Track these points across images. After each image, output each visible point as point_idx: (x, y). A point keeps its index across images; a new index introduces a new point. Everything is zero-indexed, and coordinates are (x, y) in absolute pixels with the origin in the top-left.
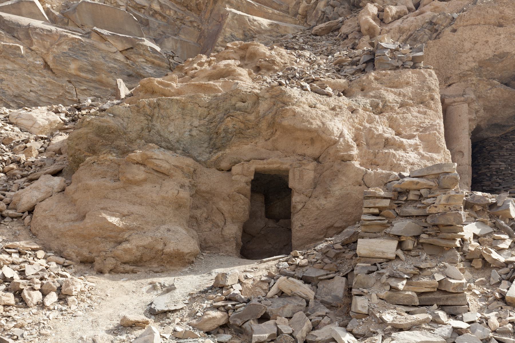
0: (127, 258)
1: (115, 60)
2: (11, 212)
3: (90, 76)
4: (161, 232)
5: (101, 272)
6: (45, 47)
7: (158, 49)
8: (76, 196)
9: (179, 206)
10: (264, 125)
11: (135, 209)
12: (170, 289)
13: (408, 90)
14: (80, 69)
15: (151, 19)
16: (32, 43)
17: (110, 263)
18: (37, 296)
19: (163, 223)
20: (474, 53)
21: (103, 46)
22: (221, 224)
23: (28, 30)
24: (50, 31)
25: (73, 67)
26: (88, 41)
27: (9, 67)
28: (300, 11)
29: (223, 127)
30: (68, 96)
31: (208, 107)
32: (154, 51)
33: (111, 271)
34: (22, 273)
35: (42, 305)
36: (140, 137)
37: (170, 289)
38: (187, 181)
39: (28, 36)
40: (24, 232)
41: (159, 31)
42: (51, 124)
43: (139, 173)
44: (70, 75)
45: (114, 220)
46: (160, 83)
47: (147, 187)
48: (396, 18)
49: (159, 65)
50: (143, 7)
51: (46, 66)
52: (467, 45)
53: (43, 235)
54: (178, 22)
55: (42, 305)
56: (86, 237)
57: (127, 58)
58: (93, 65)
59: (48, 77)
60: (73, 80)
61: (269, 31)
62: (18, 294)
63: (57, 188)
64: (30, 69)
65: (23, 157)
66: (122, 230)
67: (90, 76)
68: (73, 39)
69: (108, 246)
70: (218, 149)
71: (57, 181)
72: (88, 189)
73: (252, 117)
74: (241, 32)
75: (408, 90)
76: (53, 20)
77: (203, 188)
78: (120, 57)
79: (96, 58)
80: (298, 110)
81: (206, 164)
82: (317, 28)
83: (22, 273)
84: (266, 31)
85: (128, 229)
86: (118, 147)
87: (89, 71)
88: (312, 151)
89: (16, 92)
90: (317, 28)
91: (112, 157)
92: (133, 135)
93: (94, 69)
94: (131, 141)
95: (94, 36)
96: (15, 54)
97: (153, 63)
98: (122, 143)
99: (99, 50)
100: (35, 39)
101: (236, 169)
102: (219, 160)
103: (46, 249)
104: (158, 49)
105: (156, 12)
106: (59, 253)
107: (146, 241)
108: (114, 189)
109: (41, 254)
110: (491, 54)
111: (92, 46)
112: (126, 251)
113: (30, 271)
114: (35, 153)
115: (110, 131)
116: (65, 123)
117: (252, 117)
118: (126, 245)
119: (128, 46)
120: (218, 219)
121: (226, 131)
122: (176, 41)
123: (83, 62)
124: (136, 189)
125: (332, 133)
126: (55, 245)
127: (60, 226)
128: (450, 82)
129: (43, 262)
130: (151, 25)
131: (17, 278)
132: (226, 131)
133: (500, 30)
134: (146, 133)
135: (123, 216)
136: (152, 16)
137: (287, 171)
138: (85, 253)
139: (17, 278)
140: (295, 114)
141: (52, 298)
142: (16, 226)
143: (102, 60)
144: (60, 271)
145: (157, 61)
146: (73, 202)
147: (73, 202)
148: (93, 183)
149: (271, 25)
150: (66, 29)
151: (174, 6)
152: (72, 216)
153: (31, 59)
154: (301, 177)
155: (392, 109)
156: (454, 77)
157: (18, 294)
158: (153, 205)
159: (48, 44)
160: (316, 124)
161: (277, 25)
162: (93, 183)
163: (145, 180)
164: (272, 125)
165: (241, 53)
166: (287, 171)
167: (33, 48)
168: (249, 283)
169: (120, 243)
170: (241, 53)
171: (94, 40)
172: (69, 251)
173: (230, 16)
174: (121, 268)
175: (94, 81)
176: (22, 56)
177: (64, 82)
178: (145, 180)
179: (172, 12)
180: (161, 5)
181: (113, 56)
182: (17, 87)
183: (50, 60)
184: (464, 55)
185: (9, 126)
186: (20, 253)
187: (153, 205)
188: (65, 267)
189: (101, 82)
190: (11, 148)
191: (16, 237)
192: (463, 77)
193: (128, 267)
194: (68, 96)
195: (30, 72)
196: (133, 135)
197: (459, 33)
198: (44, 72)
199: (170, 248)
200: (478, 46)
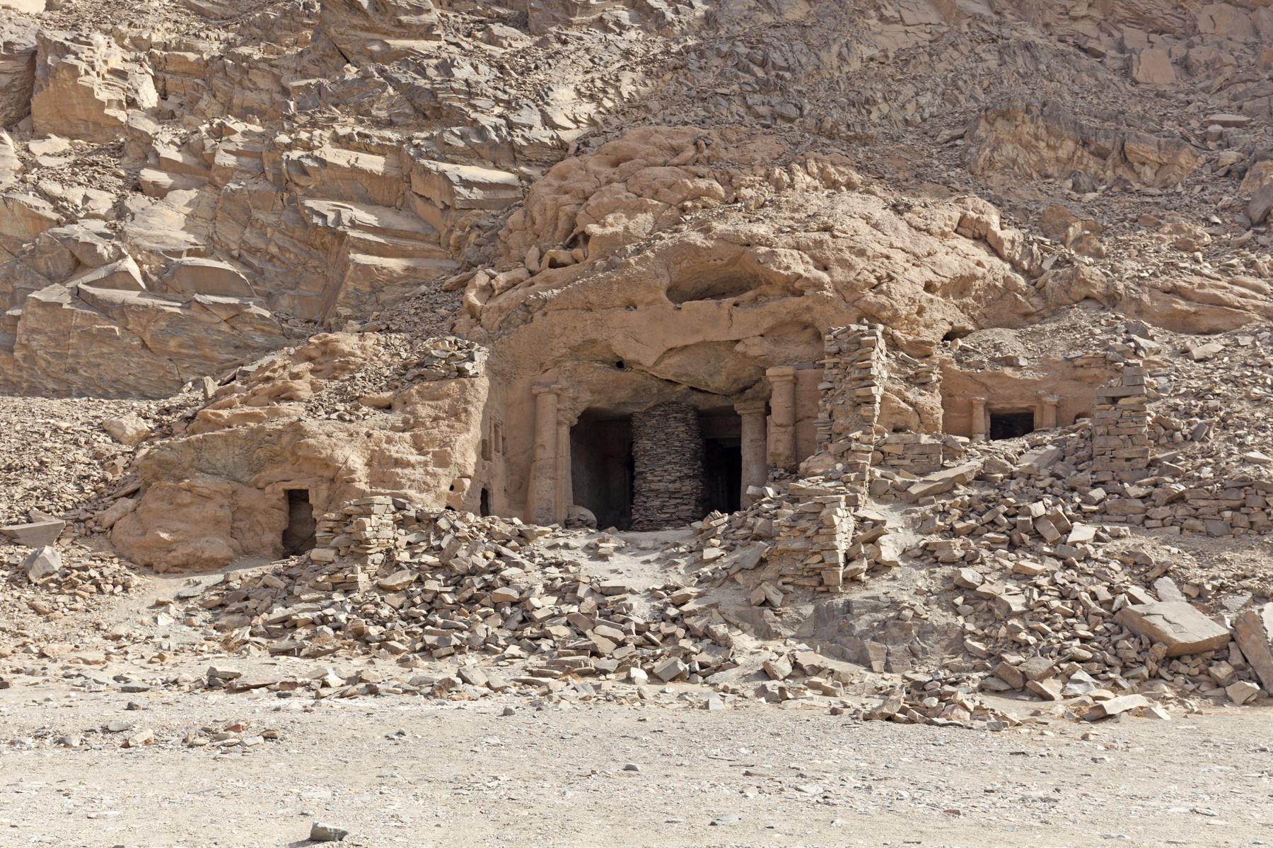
0: (176, 562)
1: (219, 331)
2: (98, 528)
3: (193, 352)
4: (201, 543)
5: (157, 573)
6: (141, 325)
7: (267, 314)
8: (143, 516)
9: (218, 522)
10: (287, 454)
11: (182, 526)
12: (197, 584)
13: (446, 403)
14: (181, 346)
15: (269, 267)
16: (128, 323)
17: (163, 566)
18: (109, 587)
19: (204, 536)
20: (564, 339)
21: (204, 317)
22: (260, 532)
23: (124, 307)
24: (146, 307)
25: (172, 344)
26: (187, 313)
27: (105, 350)
28: (452, 242)
29: (255, 456)
30: (169, 376)
31: (245, 438)
32: (262, 317)
33: (164, 572)
34: (101, 574)
35: (112, 593)
36: (192, 467)
37: (197, 584)
38: (226, 502)
39: (123, 315)
40: (107, 544)
41: (277, 281)
42: (138, 433)
43: (186, 498)
44: (170, 353)
45: (164, 536)
46: (213, 414)
47: (193, 508)
48: (506, 289)
49: (271, 333)
50: (259, 250)
51: (144, 345)
52: (558, 331)
53: (119, 546)
54: (300, 268)
55: (112, 593)
56: (147, 548)
57: (233, 328)
58: (194, 339)
59: (146, 357)
60: (174, 357)
61: (405, 277)
62: (98, 586)
63: (130, 508)
64: (127, 351)
65: (110, 476)
66: (171, 543)
67: (193, 352)
68: (171, 313)
69: (162, 554)
70: (256, 472)
71: (130, 503)
72: (150, 511)
73: (277, 448)
74: (367, 283)
75: (446, 403)
76: (151, 289)
77: (244, 505)
78: (225, 328)
79: (198, 332)
80: (311, 441)
81: (248, 485)
82: (447, 282)
83: (101, 574)
84: (400, 278)
85: (175, 541)
86: (174, 475)
87: (190, 347)
88: (328, 474)
89: (115, 376)
90: (447, 282)
91: (171, 483)
92: (186, 465)
93: (197, 343)
94: (185, 470)
95: (195, 307)
96: (110, 337)
97: (263, 331)
98: (177, 472)
99: (199, 322)
100: (130, 317)
101: (268, 489)
102: (256, 482)
103: (120, 556)
104: (267, 314)
105: (273, 257)
106: (129, 560)
107: (189, 550)
108: (168, 511)
109: (116, 560)
110: (580, 341)
111: (193, 319)
112: (174, 557)
113: (106, 572)
114: (120, 470)
115: (167, 462)
116: (152, 431)
117: (277, 448)
118: (173, 554)
119: (233, 313)
120: (258, 529)
121: (258, 458)
122: (293, 297)
123: (184, 338)
124: (185, 510)
125: (337, 461)
126: (127, 553)
127: (131, 540)
128: (545, 368)
129: (117, 566)
130: (267, 274)
131: (98, 577)
132: (258, 458)
133: (587, 315)
134: (196, 463)
135: (172, 532)
136: (270, 260)
137: (307, 491)
138: (147, 559)
139: (98, 577)
140: (308, 446)
141: (120, 588)
142: (101, 539)
143: (204, 334)
144: (127, 572)
145: (267, 329)
146: (140, 521)
147: (140, 521)
148: (153, 506)
149: (407, 269)
150: (164, 299)
151: (295, 246)
152: (139, 532)
153: (127, 340)
154: (317, 495)
155: (423, 424)
156: (548, 363)
157: (98, 586)
158: (196, 523)
159: (144, 321)
160: (326, 453)
161: (415, 269)
162: (153, 506)
163: (191, 503)
164: (294, 454)
165: (323, 348)
166: (307, 491)
167: (130, 327)
168: (247, 579)
169: (170, 551)
170: (323, 348)
171: (194, 311)
172: (136, 558)
173: (352, 267)
174: (172, 569)
175: (197, 357)
176: (118, 338)
177: (164, 361)
178: (191, 503)
179: (292, 256)
180: (280, 248)
181: (216, 327)
182: (115, 371)
183: (147, 338)
184: (555, 341)
185: (102, 435)
186: (102, 560)
187: (196, 523)
188: (132, 569)
189: (205, 358)
190: (102, 464)
191: (101, 548)
192: (556, 363)
193: (177, 569)
194: (169, 376)
195: (127, 354)
196: (186, 465)
197: (548, 317)
198: (143, 352)
199: (207, 555)
200: (567, 332)
